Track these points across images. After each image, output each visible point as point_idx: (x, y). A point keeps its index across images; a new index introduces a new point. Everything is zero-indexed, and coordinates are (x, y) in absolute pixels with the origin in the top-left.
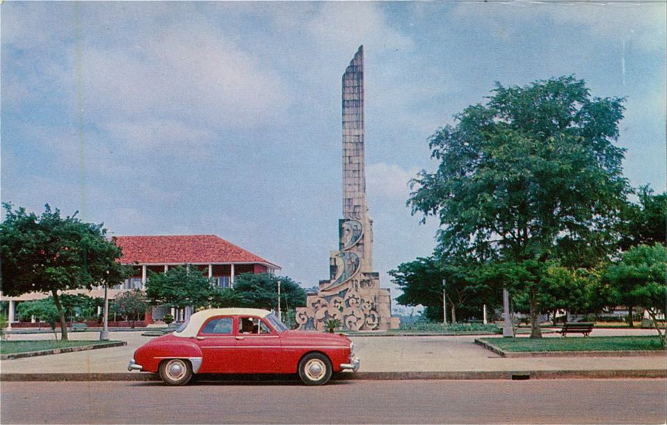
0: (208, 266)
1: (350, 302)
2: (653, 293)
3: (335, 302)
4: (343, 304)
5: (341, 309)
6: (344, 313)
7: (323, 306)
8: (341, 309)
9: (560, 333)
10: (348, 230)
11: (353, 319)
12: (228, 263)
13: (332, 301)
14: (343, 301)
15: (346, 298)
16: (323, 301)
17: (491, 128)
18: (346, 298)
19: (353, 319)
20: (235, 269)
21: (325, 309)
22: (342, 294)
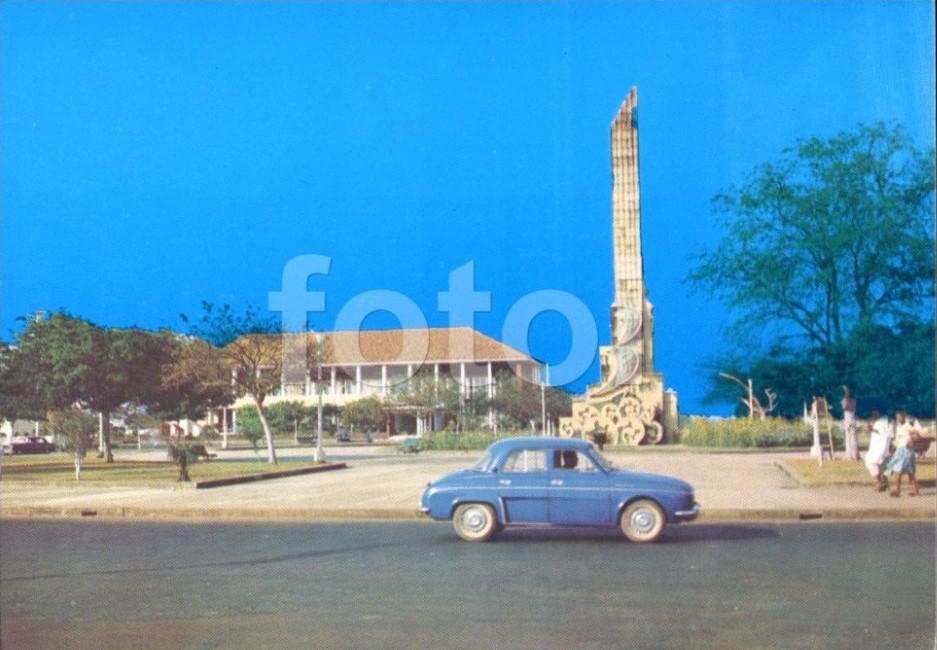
0: (381, 366)
1: (627, 410)
2: (615, 309)
3: (608, 410)
4: (618, 414)
5: (615, 420)
6: (619, 424)
7: (592, 416)
8: (615, 420)
9: (882, 467)
10: (622, 320)
11: (630, 431)
12: (376, 363)
13: (604, 409)
14: (618, 409)
15: (622, 404)
16: (593, 410)
17: (593, 474)
18: (622, 404)
19: (630, 431)
20: (466, 369)
21: (595, 419)
22: (616, 401)
